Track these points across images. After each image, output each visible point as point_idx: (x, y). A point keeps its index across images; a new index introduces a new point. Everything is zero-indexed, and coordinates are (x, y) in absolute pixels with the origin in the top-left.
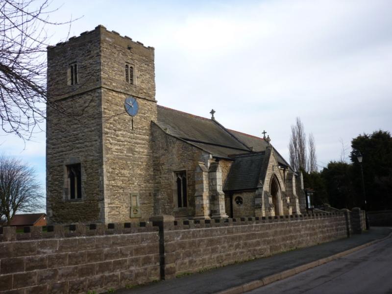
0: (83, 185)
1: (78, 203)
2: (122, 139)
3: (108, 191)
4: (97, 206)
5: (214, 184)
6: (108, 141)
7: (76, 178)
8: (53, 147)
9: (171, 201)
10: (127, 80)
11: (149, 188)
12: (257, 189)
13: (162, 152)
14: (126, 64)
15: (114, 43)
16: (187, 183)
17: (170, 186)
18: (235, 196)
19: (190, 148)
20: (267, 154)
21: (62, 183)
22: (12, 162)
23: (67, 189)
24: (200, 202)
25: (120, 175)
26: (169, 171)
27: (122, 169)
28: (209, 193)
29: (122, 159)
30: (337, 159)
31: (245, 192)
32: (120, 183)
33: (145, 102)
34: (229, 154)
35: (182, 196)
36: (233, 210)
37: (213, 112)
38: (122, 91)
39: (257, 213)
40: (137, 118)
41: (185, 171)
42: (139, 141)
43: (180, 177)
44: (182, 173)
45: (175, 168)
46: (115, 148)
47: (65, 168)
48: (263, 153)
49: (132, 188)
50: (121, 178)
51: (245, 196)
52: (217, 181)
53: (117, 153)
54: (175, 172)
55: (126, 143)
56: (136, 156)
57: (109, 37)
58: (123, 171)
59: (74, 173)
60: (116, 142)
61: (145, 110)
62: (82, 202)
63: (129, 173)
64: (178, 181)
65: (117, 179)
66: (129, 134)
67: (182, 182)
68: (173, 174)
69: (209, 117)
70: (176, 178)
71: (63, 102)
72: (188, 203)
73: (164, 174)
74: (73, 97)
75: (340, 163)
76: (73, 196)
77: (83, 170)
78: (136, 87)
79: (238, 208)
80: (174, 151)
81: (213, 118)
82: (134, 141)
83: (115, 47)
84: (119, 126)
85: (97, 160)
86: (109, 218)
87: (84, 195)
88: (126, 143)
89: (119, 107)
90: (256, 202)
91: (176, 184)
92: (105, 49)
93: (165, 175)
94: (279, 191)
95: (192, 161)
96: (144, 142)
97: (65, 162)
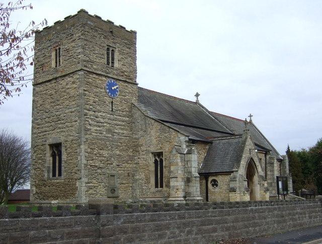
2: (102, 120)
7: (57, 157)
10: (108, 64)
11: (127, 168)
12: (233, 172)
16: (164, 165)
18: (210, 179)
21: (45, 162)
23: (49, 167)
26: (147, 151)
27: (101, 149)
35: (159, 177)
36: (209, 192)
42: (120, 123)
43: (158, 159)
44: (160, 154)
47: (48, 147)
54: (152, 153)
58: (101, 151)
59: (56, 152)
60: (96, 123)
69: (194, 100)
70: (154, 159)
74: (56, 78)
76: (54, 175)
77: (63, 150)
81: (197, 100)
84: (98, 107)
86: (86, 196)
87: (64, 174)
94: (256, 175)
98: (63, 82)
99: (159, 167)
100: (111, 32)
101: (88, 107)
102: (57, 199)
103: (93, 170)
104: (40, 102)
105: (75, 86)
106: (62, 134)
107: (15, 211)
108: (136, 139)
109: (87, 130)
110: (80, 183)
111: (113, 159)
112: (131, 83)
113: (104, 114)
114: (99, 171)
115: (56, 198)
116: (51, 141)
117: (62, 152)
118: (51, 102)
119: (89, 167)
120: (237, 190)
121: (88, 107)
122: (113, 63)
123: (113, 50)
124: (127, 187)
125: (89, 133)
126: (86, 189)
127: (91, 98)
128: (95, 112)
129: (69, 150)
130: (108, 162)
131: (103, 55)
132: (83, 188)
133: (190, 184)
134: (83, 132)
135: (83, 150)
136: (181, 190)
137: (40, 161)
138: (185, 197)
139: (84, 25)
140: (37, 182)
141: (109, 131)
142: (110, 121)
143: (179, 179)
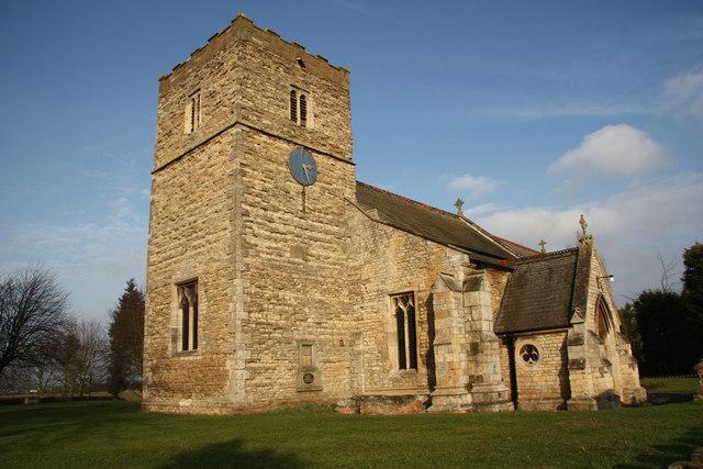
0: (200, 318)
1: (191, 358)
2: (281, 228)
3: (246, 333)
4: (224, 365)
5: (475, 317)
6: (248, 230)
7: (191, 309)
8: (157, 250)
9: (384, 356)
10: (294, 118)
12: (571, 326)
13: (365, 255)
14: (291, 89)
15: (266, 49)
16: (417, 319)
17: (382, 325)
18: (519, 344)
19: (421, 243)
20: (582, 253)
21: (168, 320)
22: (47, 272)
23: (176, 330)
24: (445, 359)
25: (273, 301)
26: (381, 293)
27: (280, 289)
28: (628, 306)
29: (279, 268)
30: (653, 284)
31: (544, 334)
32: (274, 319)
33: (331, 161)
34: (398, 367)
35: (407, 345)
36: (518, 374)
37: (459, 204)
38: (281, 135)
39: (574, 380)
40: (314, 190)
41: (412, 292)
43: (402, 307)
44: (407, 297)
45: (392, 287)
46: (263, 244)
47: (175, 289)
48: (575, 251)
49: (300, 328)
50: (279, 308)
51: (548, 344)
52: (483, 310)
53: (269, 256)
55: (289, 237)
56: (310, 263)
57: (260, 38)
58: (281, 293)
59: (189, 299)
60: (268, 233)
61: (332, 177)
62: (199, 358)
63: (296, 298)
64: (399, 314)
65: (268, 310)
66: (295, 219)
67: (406, 315)
68: (388, 300)
69: (454, 211)
70: (394, 308)
71: (176, 165)
72: (419, 360)
73: (371, 300)
74: (191, 151)
75: (659, 293)
76: (185, 346)
77: (201, 291)
78: (310, 133)
79: (527, 369)
80: (389, 253)
82: (308, 233)
83: (270, 57)
84: (273, 202)
85: (226, 268)
86: (246, 391)
87: (202, 343)
88: (289, 237)
89: (275, 165)
90: (571, 356)
91: (395, 319)
92: (249, 57)
93: (372, 304)
95: (425, 271)
96: (328, 237)
97: (173, 277)
98: (202, 157)
99: (406, 325)
100: (301, 62)
101: (250, 198)
102: (190, 397)
103: (260, 336)
104: (163, 203)
105: (223, 158)
106: (200, 258)
107: (293, 391)
108: (355, 268)
109: (247, 246)
110: (234, 362)
111: (307, 310)
112: (341, 160)
113: (287, 216)
114: (277, 335)
115: (187, 394)
116: (180, 276)
117: (199, 295)
118: (181, 199)
119: (254, 326)
120: (587, 365)
121: (250, 198)
122: (303, 119)
123: (302, 97)
124: (337, 369)
125: (251, 252)
126: (246, 375)
127: (256, 182)
128: (265, 210)
129: (212, 292)
130: (297, 314)
131: (283, 100)
132: (239, 373)
133: (480, 357)
134: (239, 251)
135: (239, 290)
136: (460, 372)
137: (160, 319)
138: (469, 387)
139: (244, 42)
140: (155, 362)
141: (297, 251)
142: (298, 231)
143: (456, 347)
